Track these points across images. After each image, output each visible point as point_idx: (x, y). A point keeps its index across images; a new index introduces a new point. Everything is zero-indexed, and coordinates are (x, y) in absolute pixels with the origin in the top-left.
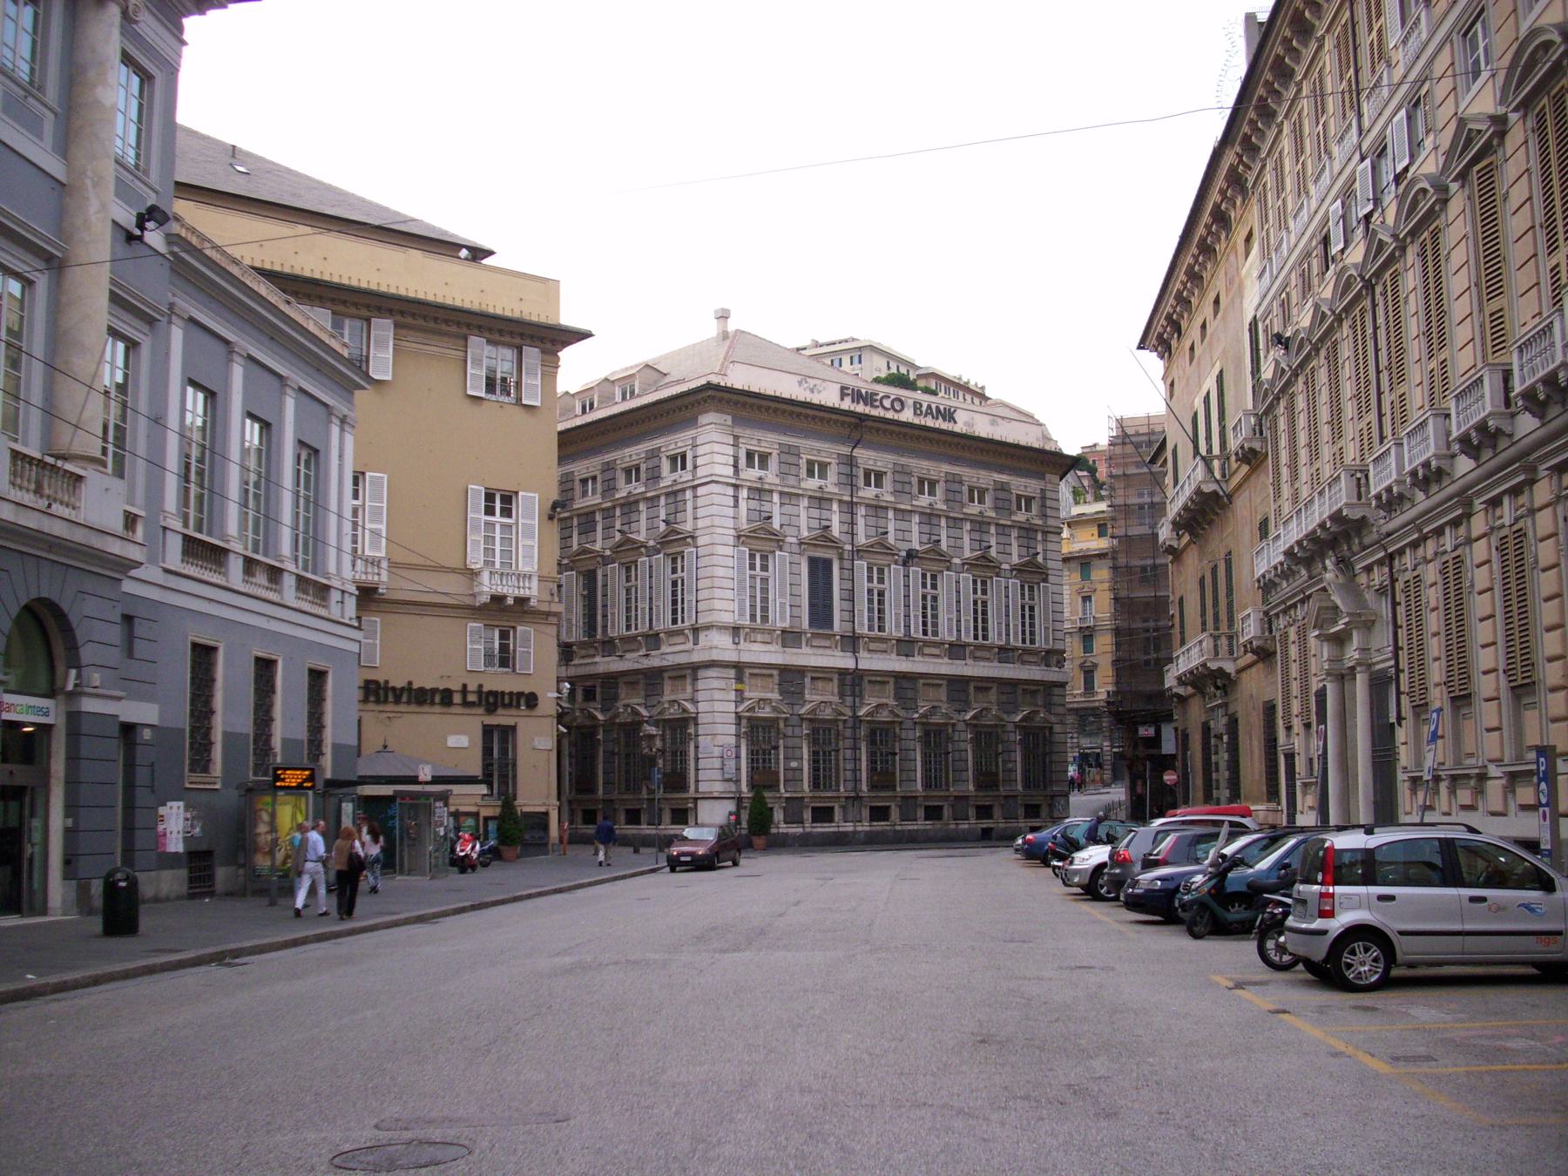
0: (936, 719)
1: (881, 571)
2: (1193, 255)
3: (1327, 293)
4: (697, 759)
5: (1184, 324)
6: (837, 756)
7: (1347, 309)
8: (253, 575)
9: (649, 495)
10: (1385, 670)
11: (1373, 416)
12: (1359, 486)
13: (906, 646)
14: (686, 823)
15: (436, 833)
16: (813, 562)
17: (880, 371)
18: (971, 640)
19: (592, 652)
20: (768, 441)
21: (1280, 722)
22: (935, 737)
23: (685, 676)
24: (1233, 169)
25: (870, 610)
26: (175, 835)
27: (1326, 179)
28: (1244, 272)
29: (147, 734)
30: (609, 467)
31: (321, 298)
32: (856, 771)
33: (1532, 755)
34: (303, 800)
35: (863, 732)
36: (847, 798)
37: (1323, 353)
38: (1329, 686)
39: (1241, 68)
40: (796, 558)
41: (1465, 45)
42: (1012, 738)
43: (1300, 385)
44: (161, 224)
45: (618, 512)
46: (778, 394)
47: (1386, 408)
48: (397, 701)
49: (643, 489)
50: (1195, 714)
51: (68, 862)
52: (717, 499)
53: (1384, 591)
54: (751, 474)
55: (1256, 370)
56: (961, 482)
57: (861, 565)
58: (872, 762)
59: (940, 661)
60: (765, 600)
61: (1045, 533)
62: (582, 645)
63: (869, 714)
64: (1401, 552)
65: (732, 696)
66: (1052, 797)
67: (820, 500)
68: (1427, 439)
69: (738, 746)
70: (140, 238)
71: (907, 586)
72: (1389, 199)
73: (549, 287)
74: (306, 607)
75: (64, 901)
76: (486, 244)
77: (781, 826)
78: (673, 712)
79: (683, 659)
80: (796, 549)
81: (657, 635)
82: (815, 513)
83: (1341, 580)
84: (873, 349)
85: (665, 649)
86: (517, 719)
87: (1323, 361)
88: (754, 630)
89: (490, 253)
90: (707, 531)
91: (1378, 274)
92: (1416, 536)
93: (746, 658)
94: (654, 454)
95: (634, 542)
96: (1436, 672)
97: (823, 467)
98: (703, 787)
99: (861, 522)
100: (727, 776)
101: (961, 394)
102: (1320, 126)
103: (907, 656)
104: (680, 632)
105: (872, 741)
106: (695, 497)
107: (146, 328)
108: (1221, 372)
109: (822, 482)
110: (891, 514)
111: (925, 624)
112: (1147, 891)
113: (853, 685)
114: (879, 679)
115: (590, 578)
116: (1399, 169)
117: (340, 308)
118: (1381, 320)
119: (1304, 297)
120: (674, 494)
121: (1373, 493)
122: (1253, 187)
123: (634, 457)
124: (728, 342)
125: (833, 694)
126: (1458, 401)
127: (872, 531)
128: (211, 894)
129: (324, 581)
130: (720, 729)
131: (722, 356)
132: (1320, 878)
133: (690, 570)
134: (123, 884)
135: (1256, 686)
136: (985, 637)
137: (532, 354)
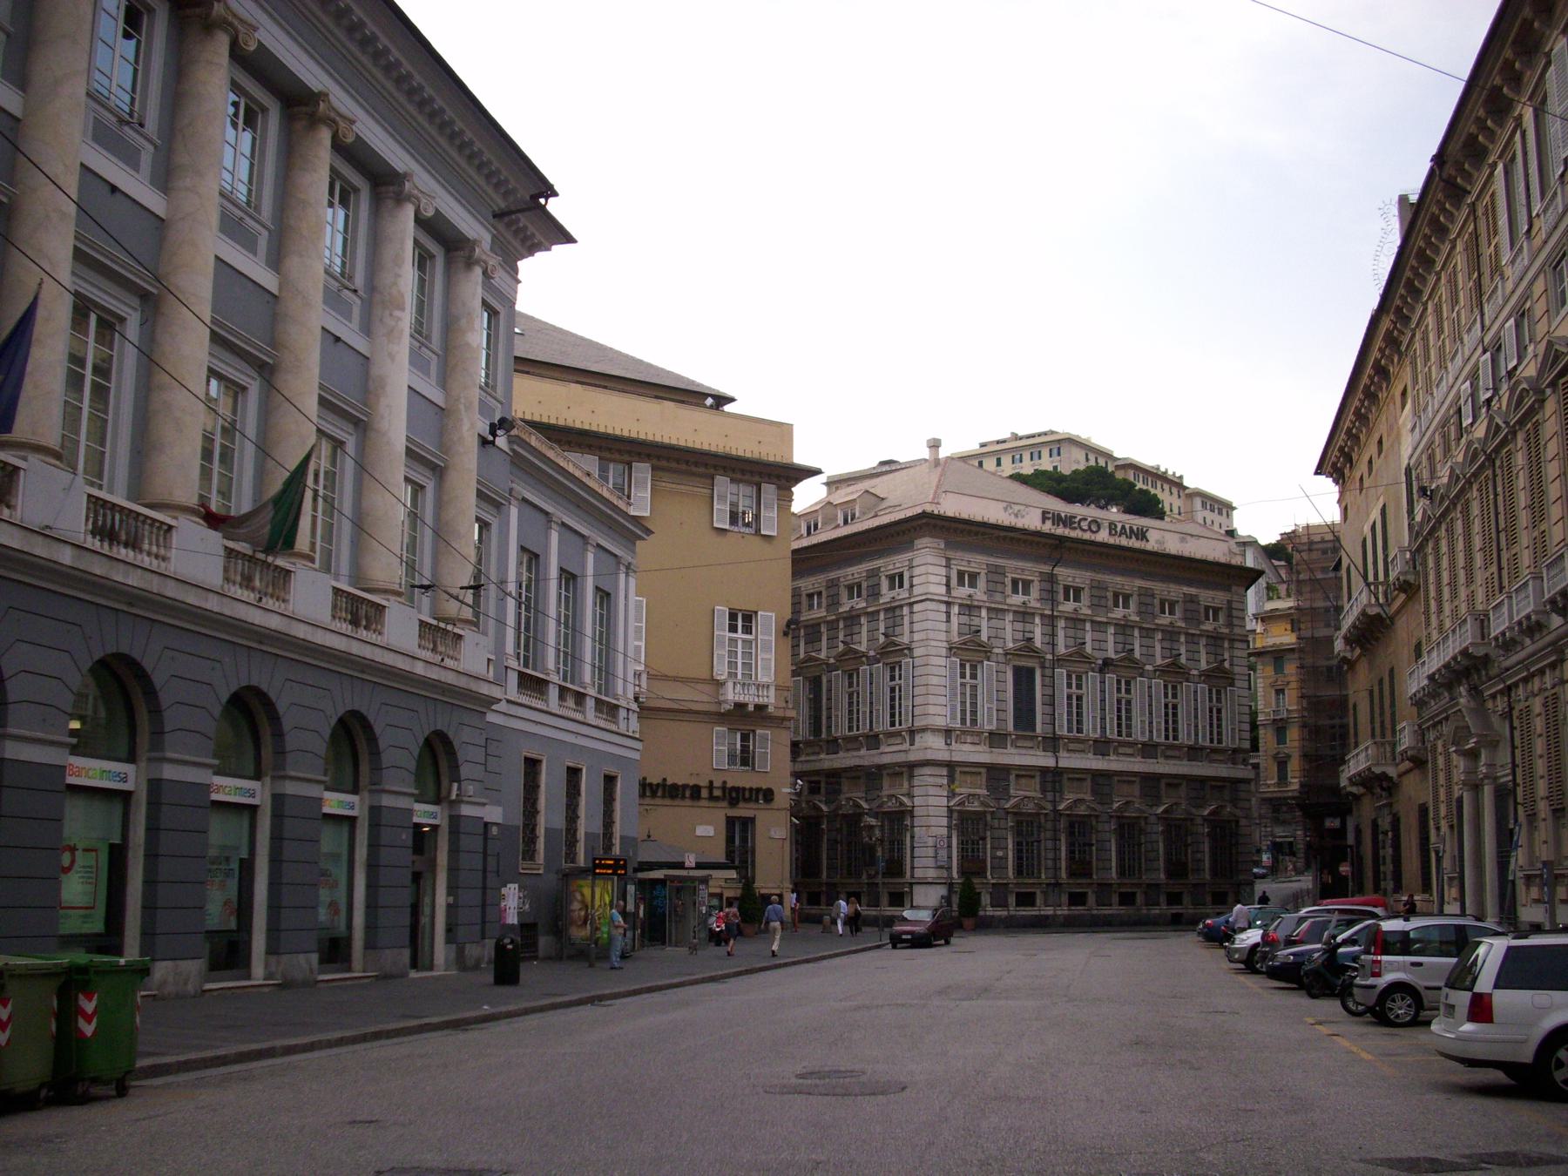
1: (1079, 678)
2: (1359, 400)
3: (1460, 459)
4: (913, 848)
5: (1355, 456)
6: (1039, 847)
7: (1475, 475)
8: (565, 701)
9: (870, 610)
10: (1505, 784)
11: (1494, 568)
12: (1482, 628)
13: (1102, 746)
14: (902, 904)
15: (700, 912)
16: (1018, 672)
17: (1078, 463)
18: (1162, 740)
19: (817, 749)
20: (978, 562)
21: (1431, 823)
22: (1128, 830)
23: (902, 773)
24: (1389, 333)
25: (1070, 713)
26: (512, 910)
27: (1459, 360)
28: (1401, 421)
29: (494, 830)
30: (833, 584)
31: (590, 447)
32: (1056, 859)
33: (1540, 865)
34: (610, 883)
35: (1063, 824)
36: (1048, 885)
37: (1459, 508)
38: (1465, 794)
39: (1395, 240)
40: (1002, 668)
41: (1555, 276)
42: (1200, 829)
43: (1457, 514)
44: (508, 431)
45: (841, 625)
46: (986, 520)
47: (1504, 563)
48: (654, 795)
49: (864, 605)
50: (1366, 811)
51: (450, 930)
52: (931, 615)
53: (1508, 715)
55: (1411, 512)
56: (1153, 596)
57: (1061, 673)
58: (1071, 852)
59: (1132, 759)
60: (974, 704)
61: (1232, 641)
62: (808, 743)
64: (1516, 685)
66: (1239, 885)
67: (1024, 615)
68: (1527, 597)
69: (949, 837)
70: (493, 443)
71: (1102, 691)
72: (1505, 387)
73: (783, 431)
74: (602, 724)
75: (447, 960)
76: (724, 389)
77: (988, 910)
78: (891, 806)
79: (901, 758)
80: (1001, 659)
82: (1019, 626)
83: (1472, 704)
84: (1072, 441)
85: (884, 748)
86: (756, 812)
87: (1475, 493)
88: (964, 732)
89: (731, 400)
90: (922, 644)
91: (1497, 450)
92: (1525, 674)
93: (957, 758)
94: (874, 573)
95: (856, 652)
96: (1542, 788)
97: (1027, 585)
98: (919, 873)
99: (1061, 634)
100: (939, 864)
102: (1455, 313)
103: (1103, 755)
104: (898, 734)
105: (1071, 834)
106: (912, 613)
107: (494, 511)
108: (1384, 505)
109: (1026, 598)
110: (1088, 626)
111: (1119, 725)
112: (1284, 964)
113: (1054, 782)
114: (1077, 776)
115: (815, 683)
116: (1510, 366)
117: (607, 455)
118: (1499, 489)
119: (1445, 457)
120: (893, 610)
121: (1492, 635)
122: (1406, 350)
123: (856, 576)
124: (939, 469)
125: (1035, 791)
126: (1548, 569)
127: (1071, 642)
128: (536, 958)
129: (582, 690)
130: (933, 821)
131: (934, 484)
132: (1373, 950)
133: (907, 678)
134: (510, 947)
135: (1414, 790)
136: (1175, 738)
137: (769, 490)
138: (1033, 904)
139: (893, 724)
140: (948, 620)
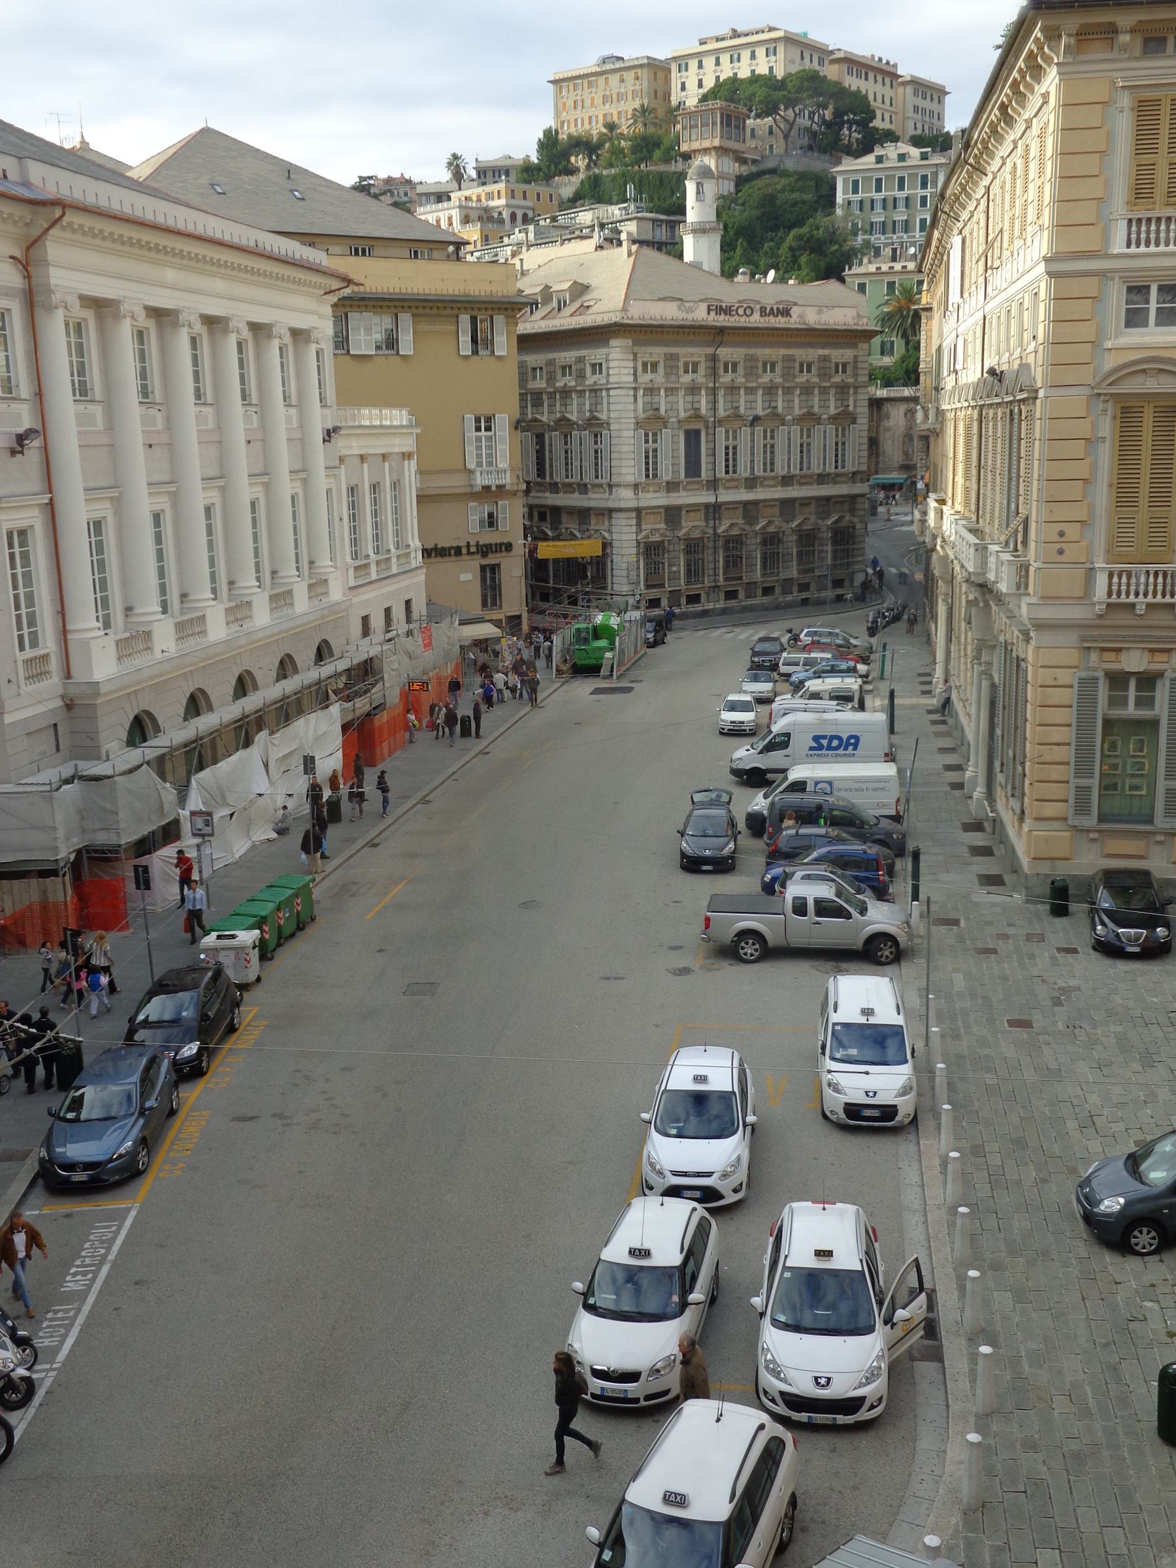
0: (771, 529)
16: (688, 433)
20: (657, 353)
22: (771, 541)
35: (721, 543)
40: (676, 432)
52: (623, 399)
54: (645, 378)
57: (721, 432)
63: (727, 531)
65: (634, 529)
67: (693, 390)
69: (638, 561)
71: (753, 440)
80: (676, 426)
81: (586, 485)
85: (591, 495)
93: (642, 504)
94: (581, 360)
97: (696, 366)
99: (721, 400)
101: (879, 78)
104: (601, 486)
105: (726, 549)
106: (608, 395)
113: (714, 513)
115: (540, 438)
127: (729, 406)
130: (625, 551)
137: (499, 320)
138: (699, 602)
139: (597, 477)
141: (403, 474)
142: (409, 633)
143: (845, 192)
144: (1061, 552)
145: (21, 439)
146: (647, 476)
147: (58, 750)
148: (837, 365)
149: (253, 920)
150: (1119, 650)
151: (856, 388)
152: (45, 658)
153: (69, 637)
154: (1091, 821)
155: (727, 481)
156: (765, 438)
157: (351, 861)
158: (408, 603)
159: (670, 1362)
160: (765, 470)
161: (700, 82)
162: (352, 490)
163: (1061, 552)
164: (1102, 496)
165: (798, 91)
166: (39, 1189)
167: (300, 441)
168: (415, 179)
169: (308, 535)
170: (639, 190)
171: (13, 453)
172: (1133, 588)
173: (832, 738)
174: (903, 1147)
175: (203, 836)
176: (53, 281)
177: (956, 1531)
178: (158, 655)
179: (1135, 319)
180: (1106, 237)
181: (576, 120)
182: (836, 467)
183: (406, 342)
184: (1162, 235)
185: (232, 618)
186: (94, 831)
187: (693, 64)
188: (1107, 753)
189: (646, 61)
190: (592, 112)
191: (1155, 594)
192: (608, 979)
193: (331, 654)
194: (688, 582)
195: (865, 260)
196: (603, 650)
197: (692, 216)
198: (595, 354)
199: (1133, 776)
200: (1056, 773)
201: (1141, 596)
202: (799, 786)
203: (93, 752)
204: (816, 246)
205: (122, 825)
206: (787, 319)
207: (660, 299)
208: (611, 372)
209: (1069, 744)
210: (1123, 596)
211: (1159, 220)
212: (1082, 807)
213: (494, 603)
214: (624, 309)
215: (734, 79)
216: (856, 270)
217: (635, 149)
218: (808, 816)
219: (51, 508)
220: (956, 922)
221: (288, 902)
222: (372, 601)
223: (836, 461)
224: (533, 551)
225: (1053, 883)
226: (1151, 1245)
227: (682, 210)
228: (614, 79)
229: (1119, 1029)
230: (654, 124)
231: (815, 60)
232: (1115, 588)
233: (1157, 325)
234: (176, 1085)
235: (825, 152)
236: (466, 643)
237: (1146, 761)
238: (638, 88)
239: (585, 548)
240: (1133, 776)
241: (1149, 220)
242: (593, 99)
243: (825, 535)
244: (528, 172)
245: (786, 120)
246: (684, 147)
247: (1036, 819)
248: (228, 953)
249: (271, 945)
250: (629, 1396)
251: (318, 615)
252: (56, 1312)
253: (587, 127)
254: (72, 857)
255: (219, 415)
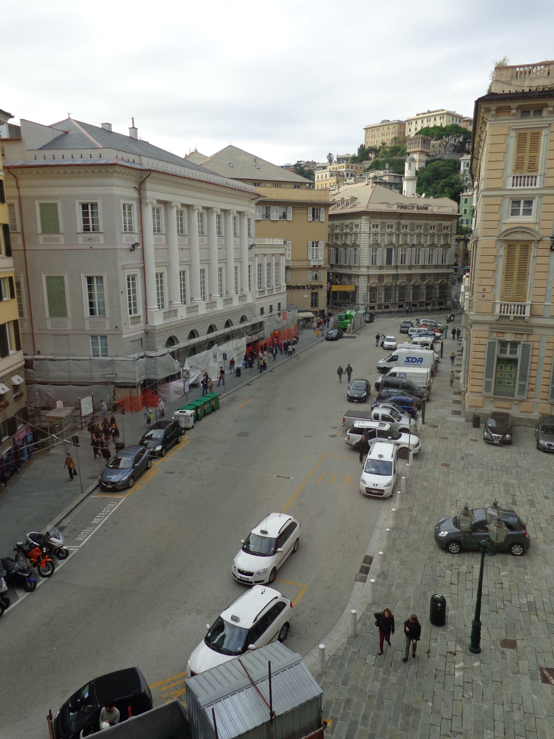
0: (417, 284)
16: (388, 250)
20: (378, 221)
22: (416, 288)
35: (398, 288)
40: (384, 249)
54: (373, 230)
57: (400, 249)
65: (367, 282)
67: (390, 234)
69: (367, 293)
80: (384, 247)
93: (370, 273)
94: (352, 223)
99: (401, 238)
104: (355, 267)
113: (396, 277)
130: (363, 290)
137: (323, 209)
140: (370, 238)
141: (280, 260)
142: (279, 314)
143: (464, 166)
144: (484, 296)
145: (133, 246)
146: (372, 264)
147: (142, 347)
148: (444, 227)
149: (194, 407)
150: (504, 333)
151: (451, 235)
152: (139, 316)
153: (148, 310)
154: (491, 394)
155: (401, 266)
156: (416, 252)
157: (239, 390)
158: (279, 304)
159: (265, 571)
160: (415, 263)
161: (416, 128)
162: (260, 265)
163: (484, 296)
164: (500, 276)
165: (451, 131)
166: (99, 489)
167: (239, 249)
168: (317, 162)
169: (241, 280)
170: (390, 165)
171: (131, 250)
172: (509, 310)
173: (413, 358)
174: (384, 505)
175: (186, 378)
176: (148, 195)
177: (343, 644)
178: (179, 318)
179: (515, 212)
180: (505, 182)
181: (372, 142)
182: (442, 263)
183: (290, 217)
184: (526, 182)
185: (209, 307)
186: (149, 374)
187: (414, 122)
188: (499, 370)
189: (397, 122)
190: (378, 139)
191: (517, 313)
192: (306, 436)
193: (247, 320)
194: (385, 301)
195: (468, 190)
196: (348, 323)
197: (406, 174)
198: (356, 221)
199: (508, 379)
200: (478, 376)
201: (512, 313)
202: (394, 374)
203: (154, 349)
204: (452, 185)
205: (158, 373)
206: (427, 211)
207: (381, 203)
208: (362, 227)
209: (484, 366)
210: (505, 313)
211: (525, 177)
212: (488, 389)
213: (315, 306)
214: (367, 207)
215: (428, 128)
216: (465, 194)
217: (391, 151)
218: (396, 386)
219: (144, 269)
220: (437, 427)
221: (209, 402)
222: (265, 303)
223: (442, 261)
224: (330, 288)
225: (474, 416)
226: (519, 552)
227: (403, 173)
228: (386, 128)
229: (481, 470)
230: (399, 143)
231: (458, 120)
232: (502, 310)
233: (523, 215)
234: (150, 459)
235: (459, 153)
236: (300, 319)
237: (513, 374)
238: (394, 131)
239: (349, 288)
240: (508, 379)
241: (521, 177)
242: (378, 134)
243: (437, 287)
244: (354, 159)
245: (446, 142)
246: (408, 151)
247: (471, 392)
248: (182, 417)
249: (201, 416)
250: (249, 581)
251: (242, 307)
252: (87, 529)
253: (375, 144)
254: (142, 382)
255: (241, 241)
